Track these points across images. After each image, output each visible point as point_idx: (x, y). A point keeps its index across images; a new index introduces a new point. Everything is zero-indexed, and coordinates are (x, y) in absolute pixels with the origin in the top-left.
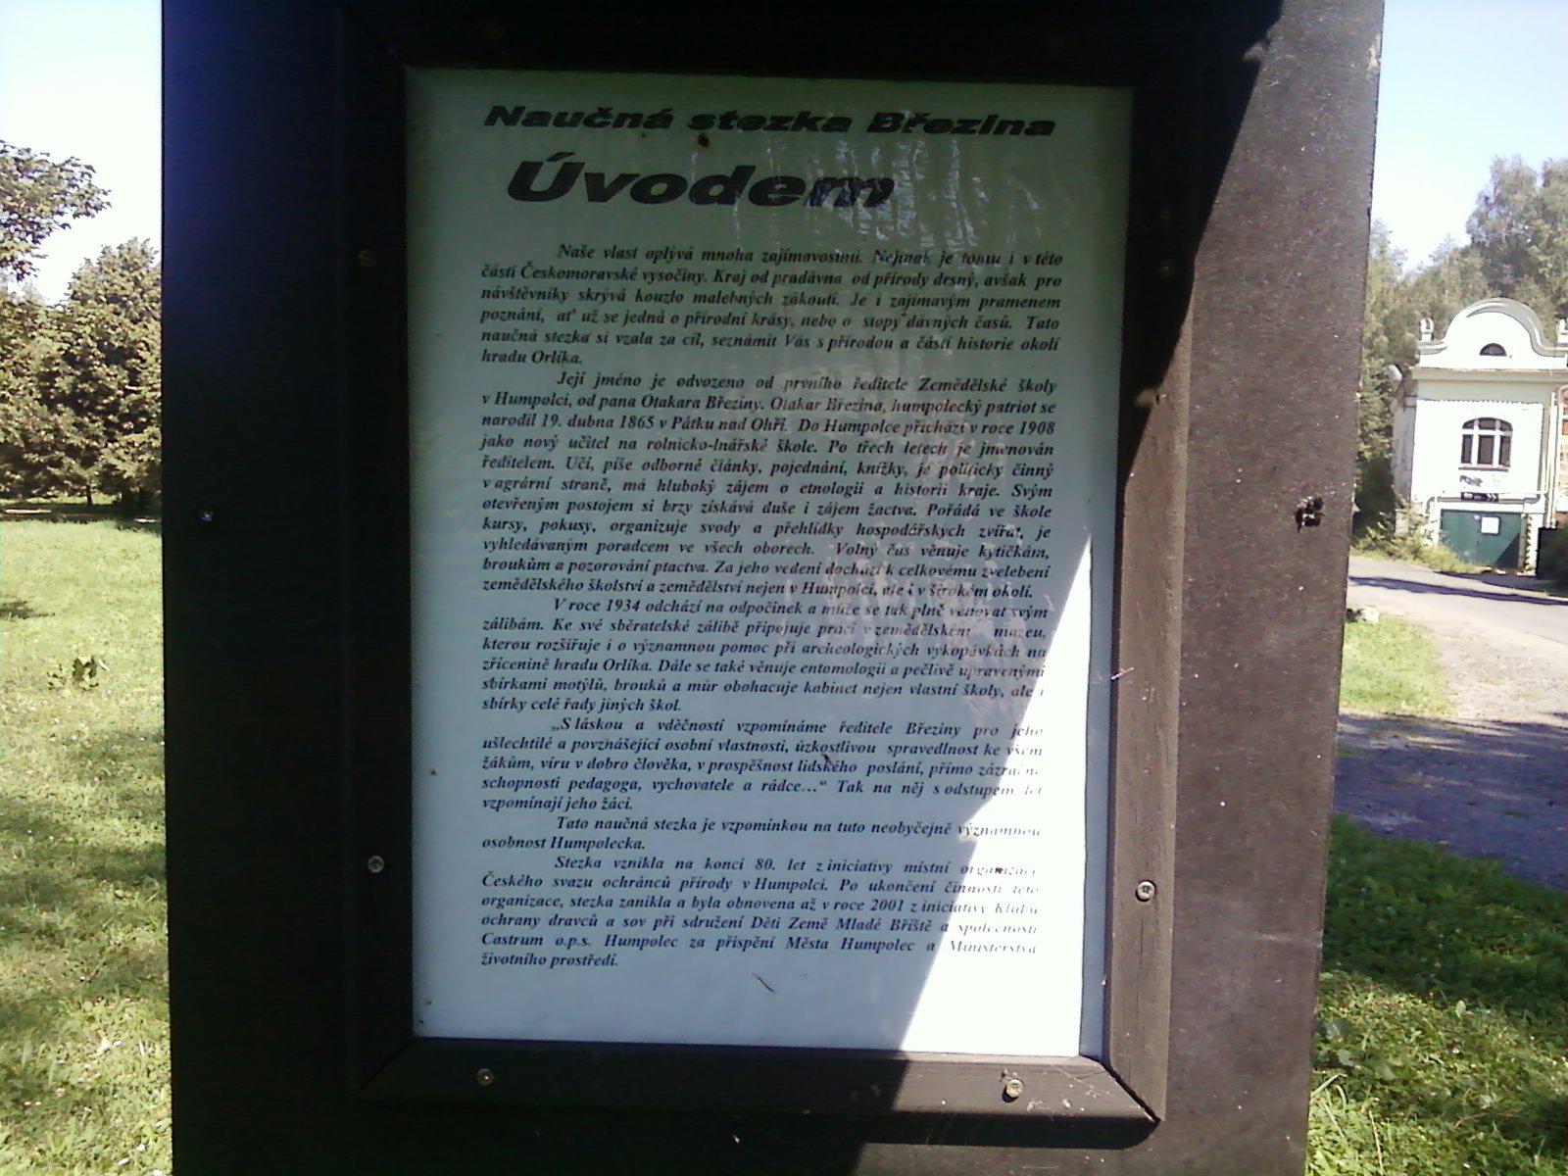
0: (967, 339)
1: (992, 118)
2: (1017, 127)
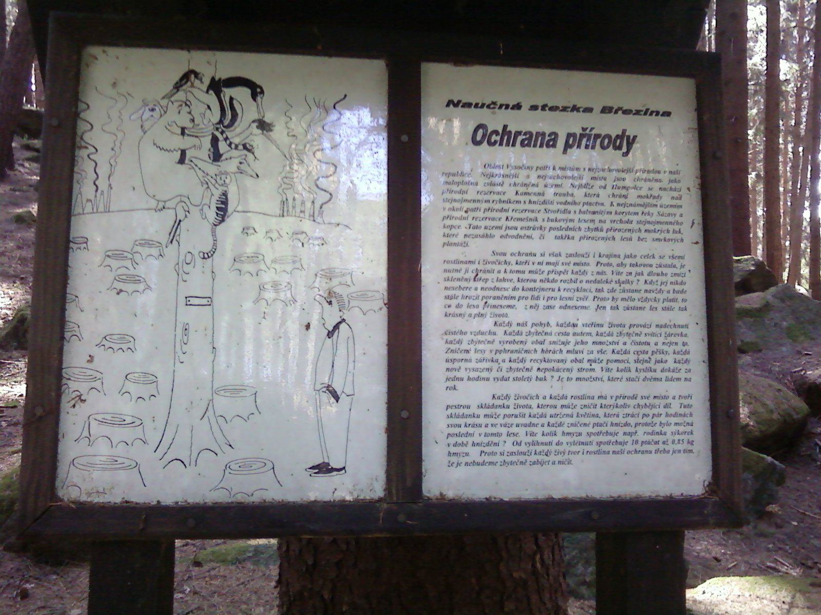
0: (545, 349)
1: (647, 110)
2: (657, 113)
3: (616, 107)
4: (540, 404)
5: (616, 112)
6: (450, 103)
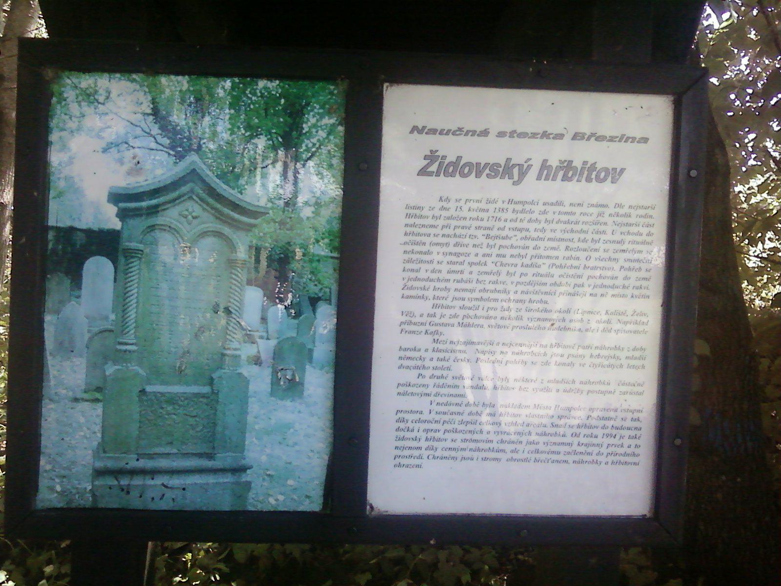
1: (623, 136)
2: (474, 133)
3: (588, 134)
4: (436, 296)
5: (589, 139)
6: (415, 129)
